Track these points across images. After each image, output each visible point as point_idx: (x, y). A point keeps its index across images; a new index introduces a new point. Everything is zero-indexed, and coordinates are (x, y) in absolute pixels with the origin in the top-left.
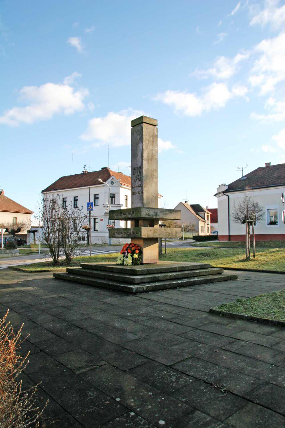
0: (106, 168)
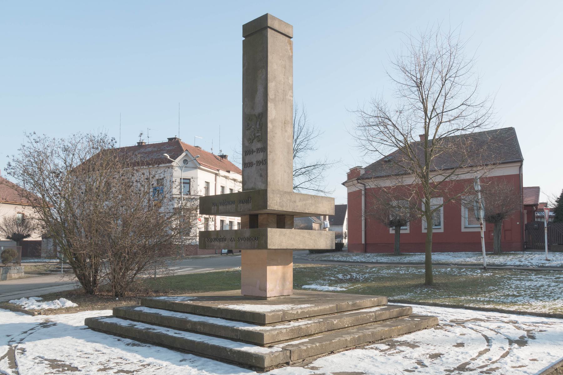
0: (175, 138)
